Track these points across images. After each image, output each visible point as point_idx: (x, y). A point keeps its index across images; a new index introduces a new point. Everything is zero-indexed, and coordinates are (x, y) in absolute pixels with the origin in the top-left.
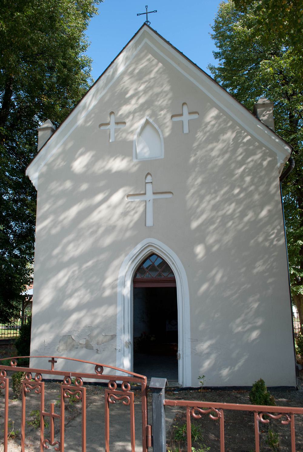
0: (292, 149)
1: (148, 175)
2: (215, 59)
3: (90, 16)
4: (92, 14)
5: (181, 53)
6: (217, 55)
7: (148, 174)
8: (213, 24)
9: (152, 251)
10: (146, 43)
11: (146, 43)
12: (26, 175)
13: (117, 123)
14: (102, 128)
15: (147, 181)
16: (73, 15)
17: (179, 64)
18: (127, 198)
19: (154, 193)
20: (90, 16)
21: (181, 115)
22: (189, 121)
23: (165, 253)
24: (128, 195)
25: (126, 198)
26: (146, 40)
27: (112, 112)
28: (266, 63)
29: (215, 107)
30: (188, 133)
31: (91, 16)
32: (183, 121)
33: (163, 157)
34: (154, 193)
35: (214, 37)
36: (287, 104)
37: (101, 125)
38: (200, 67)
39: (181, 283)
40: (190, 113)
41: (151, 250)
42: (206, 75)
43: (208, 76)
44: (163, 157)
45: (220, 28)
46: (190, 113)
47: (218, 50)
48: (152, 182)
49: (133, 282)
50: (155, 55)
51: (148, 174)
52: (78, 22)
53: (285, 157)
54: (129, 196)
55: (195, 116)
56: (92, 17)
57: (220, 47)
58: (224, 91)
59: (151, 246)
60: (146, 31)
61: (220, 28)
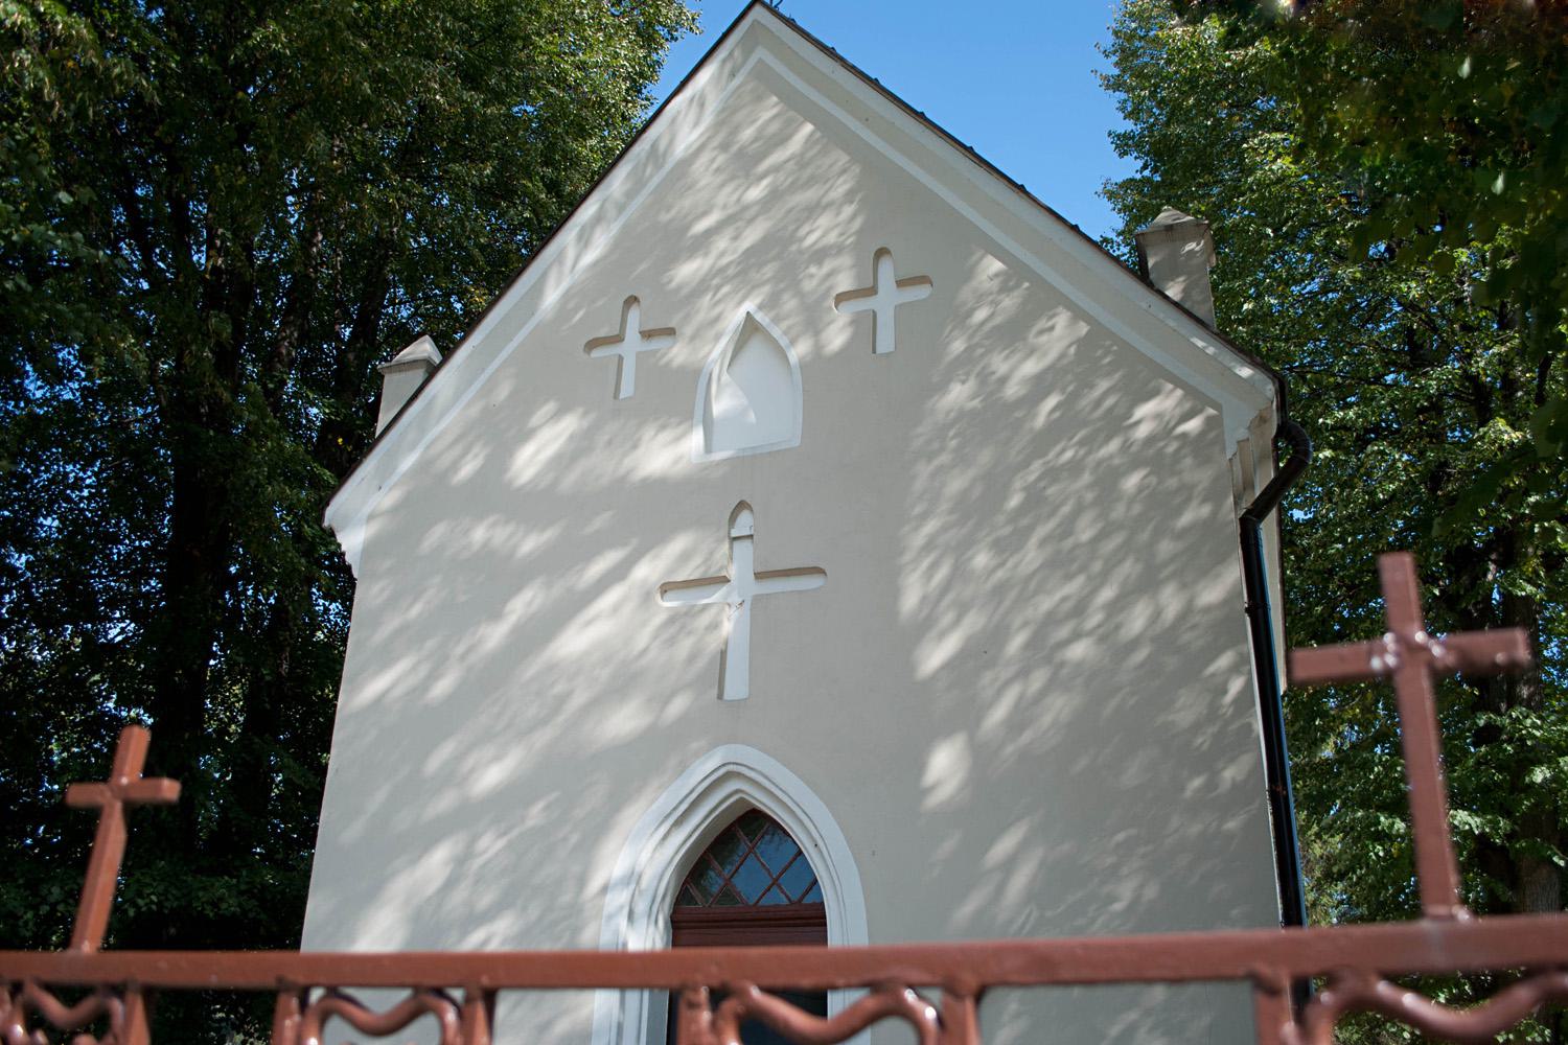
0: (1277, 385)
1: (740, 512)
2: (1122, 155)
3: (669, 37)
4: (676, 30)
5: (874, 84)
6: (1124, 144)
7: (742, 506)
8: (1109, 41)
9: (742, 798)
10: (760, 61)
11: (760, 61)
12: (326, 524)
13: (647, 335)
14: (597, 353)
15: (734, 533)
16: (624, 36)
17: (867, 120)
18: (662, 597)
19: (759, 576)
20: (669, 37)
21: (872, 291)
22: (899, 308)
23: (789, 807)
24: (663, 585)
25: (658, 596)
26: (761, 53)
27: (631, 297)
28: (1272, 145)
29: (992, 255)
30: (891, 353)
31: (672, 38)
32: (874, 313)
33: (797, 443)
34: (760, 576)
35: (1115, 85)
36: (1487, 348)
37: (593, 344)
38: (909, 103)
39: (841, 918)
40: (901, 283)
41: (737, 791)
42: (949, 141)
43: (963, 151)
44: (797, 443)
45: (1134, 54)
46: (901, 283)
47: (1129, 126)
48: (751, 536)
49: (672, 921)
50: (789, 98)
51: (742, 506)
52: (616, 52)
53: (1253, 414)
54: (671, 589)
55: (921, 293)
56: (677, 39)
57: (1134, 114)
58: (1021, 194)
59: (739, 775)
60: (759, 23)
61: (1134, 54)
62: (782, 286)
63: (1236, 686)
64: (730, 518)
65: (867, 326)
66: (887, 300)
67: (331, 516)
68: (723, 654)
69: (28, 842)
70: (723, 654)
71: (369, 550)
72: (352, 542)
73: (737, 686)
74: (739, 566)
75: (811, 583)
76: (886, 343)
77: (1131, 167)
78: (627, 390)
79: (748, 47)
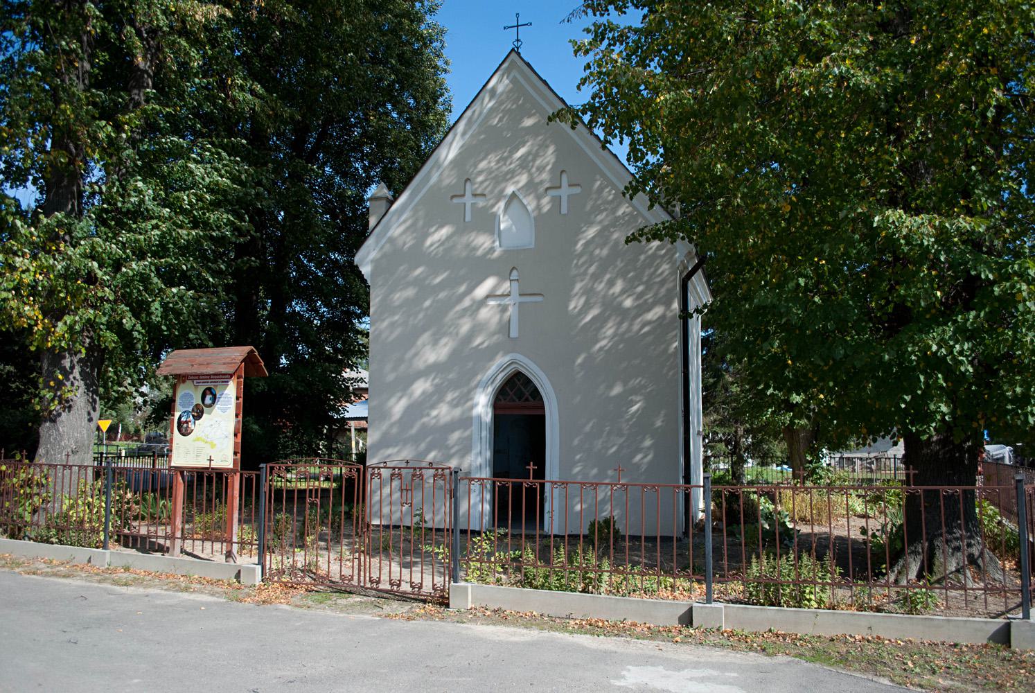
7: (514, 268)
10: (513, 60)
26: (514, 73)
33: (532, 246)
44: (532, 246)
51: (514, 268)
62: (423, 446)
63: (676, 344)
64: (537, 424)
65: (557, 201)
66: (565, 191)
67: (357, 260)
68: (509, 321)
69: (284, 361)
70: (509, 321)
71: (373, 273)
72: (366, 270)
73: (514, 333)
74: (515, 293)
75: (539, 299)
76: (564, 210)
77: (364, 325)
78: (468, 218)
79: (508, 71)
